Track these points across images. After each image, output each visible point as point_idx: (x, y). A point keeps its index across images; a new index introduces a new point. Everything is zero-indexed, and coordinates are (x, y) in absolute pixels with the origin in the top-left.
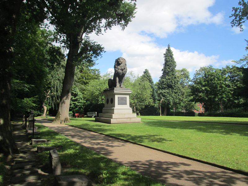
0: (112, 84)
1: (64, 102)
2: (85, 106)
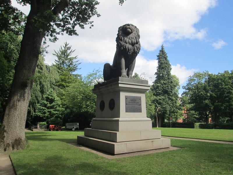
0: (112, 73)
1: (14, 106)
2: (63, 115)
